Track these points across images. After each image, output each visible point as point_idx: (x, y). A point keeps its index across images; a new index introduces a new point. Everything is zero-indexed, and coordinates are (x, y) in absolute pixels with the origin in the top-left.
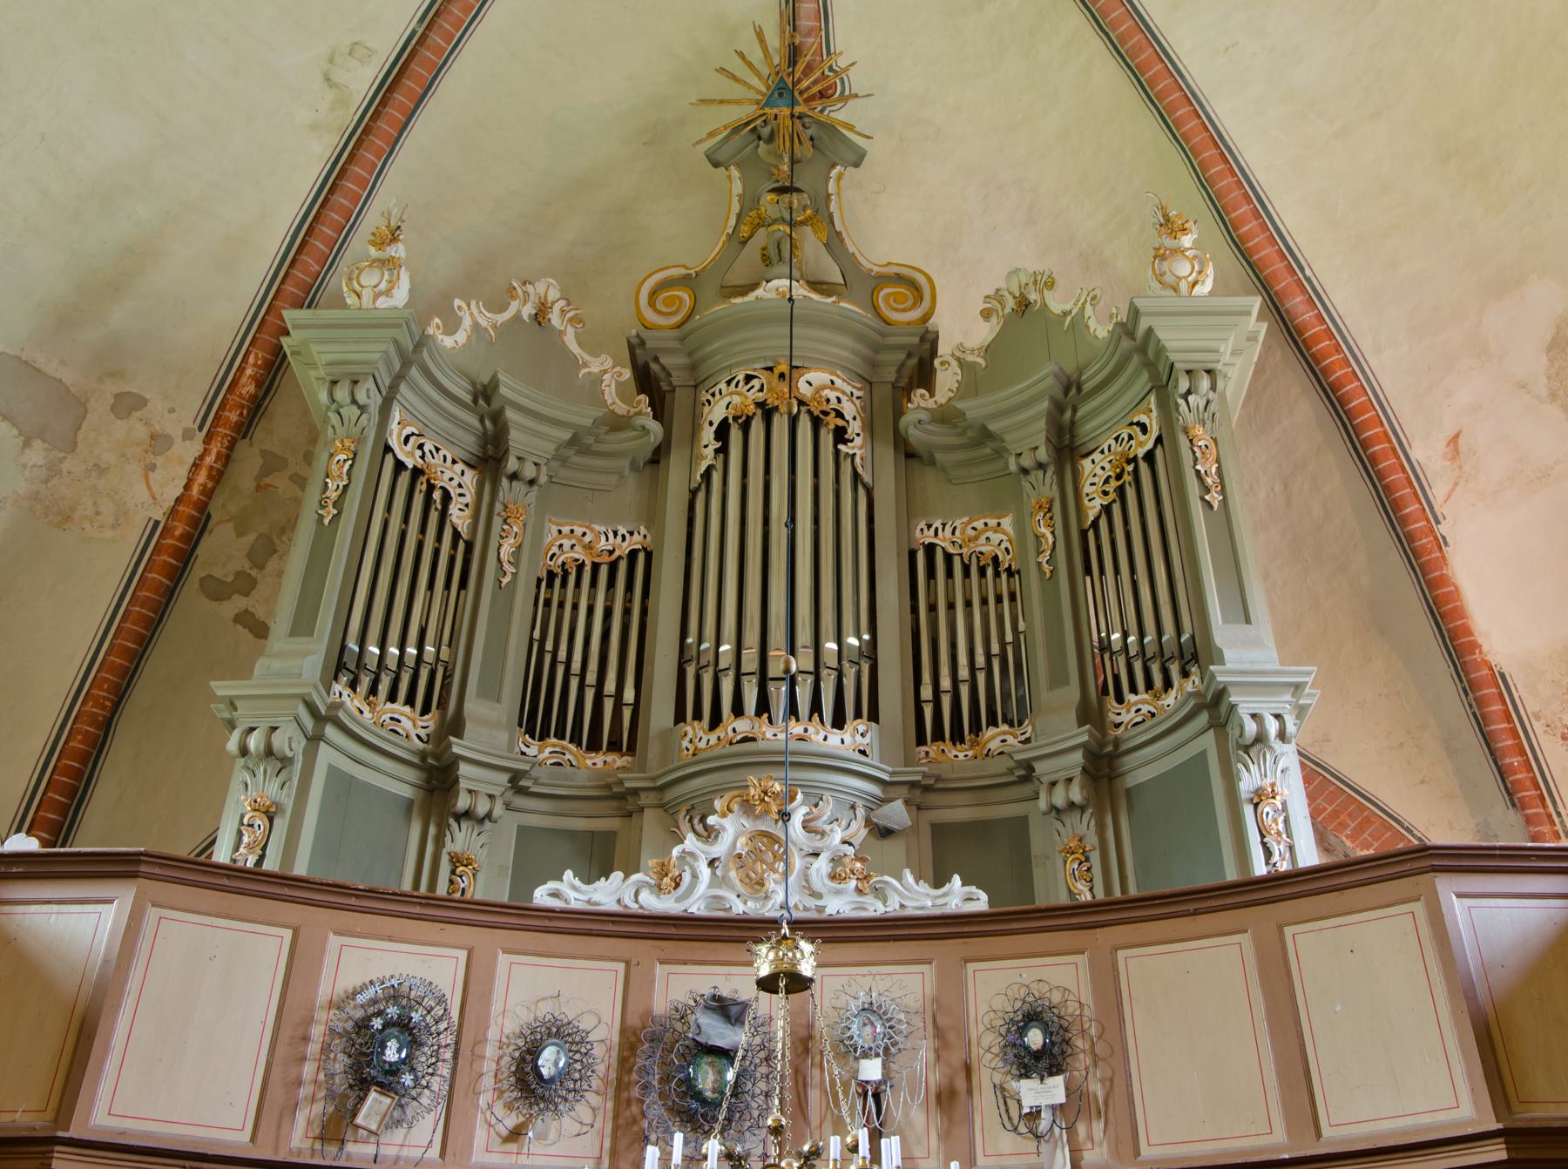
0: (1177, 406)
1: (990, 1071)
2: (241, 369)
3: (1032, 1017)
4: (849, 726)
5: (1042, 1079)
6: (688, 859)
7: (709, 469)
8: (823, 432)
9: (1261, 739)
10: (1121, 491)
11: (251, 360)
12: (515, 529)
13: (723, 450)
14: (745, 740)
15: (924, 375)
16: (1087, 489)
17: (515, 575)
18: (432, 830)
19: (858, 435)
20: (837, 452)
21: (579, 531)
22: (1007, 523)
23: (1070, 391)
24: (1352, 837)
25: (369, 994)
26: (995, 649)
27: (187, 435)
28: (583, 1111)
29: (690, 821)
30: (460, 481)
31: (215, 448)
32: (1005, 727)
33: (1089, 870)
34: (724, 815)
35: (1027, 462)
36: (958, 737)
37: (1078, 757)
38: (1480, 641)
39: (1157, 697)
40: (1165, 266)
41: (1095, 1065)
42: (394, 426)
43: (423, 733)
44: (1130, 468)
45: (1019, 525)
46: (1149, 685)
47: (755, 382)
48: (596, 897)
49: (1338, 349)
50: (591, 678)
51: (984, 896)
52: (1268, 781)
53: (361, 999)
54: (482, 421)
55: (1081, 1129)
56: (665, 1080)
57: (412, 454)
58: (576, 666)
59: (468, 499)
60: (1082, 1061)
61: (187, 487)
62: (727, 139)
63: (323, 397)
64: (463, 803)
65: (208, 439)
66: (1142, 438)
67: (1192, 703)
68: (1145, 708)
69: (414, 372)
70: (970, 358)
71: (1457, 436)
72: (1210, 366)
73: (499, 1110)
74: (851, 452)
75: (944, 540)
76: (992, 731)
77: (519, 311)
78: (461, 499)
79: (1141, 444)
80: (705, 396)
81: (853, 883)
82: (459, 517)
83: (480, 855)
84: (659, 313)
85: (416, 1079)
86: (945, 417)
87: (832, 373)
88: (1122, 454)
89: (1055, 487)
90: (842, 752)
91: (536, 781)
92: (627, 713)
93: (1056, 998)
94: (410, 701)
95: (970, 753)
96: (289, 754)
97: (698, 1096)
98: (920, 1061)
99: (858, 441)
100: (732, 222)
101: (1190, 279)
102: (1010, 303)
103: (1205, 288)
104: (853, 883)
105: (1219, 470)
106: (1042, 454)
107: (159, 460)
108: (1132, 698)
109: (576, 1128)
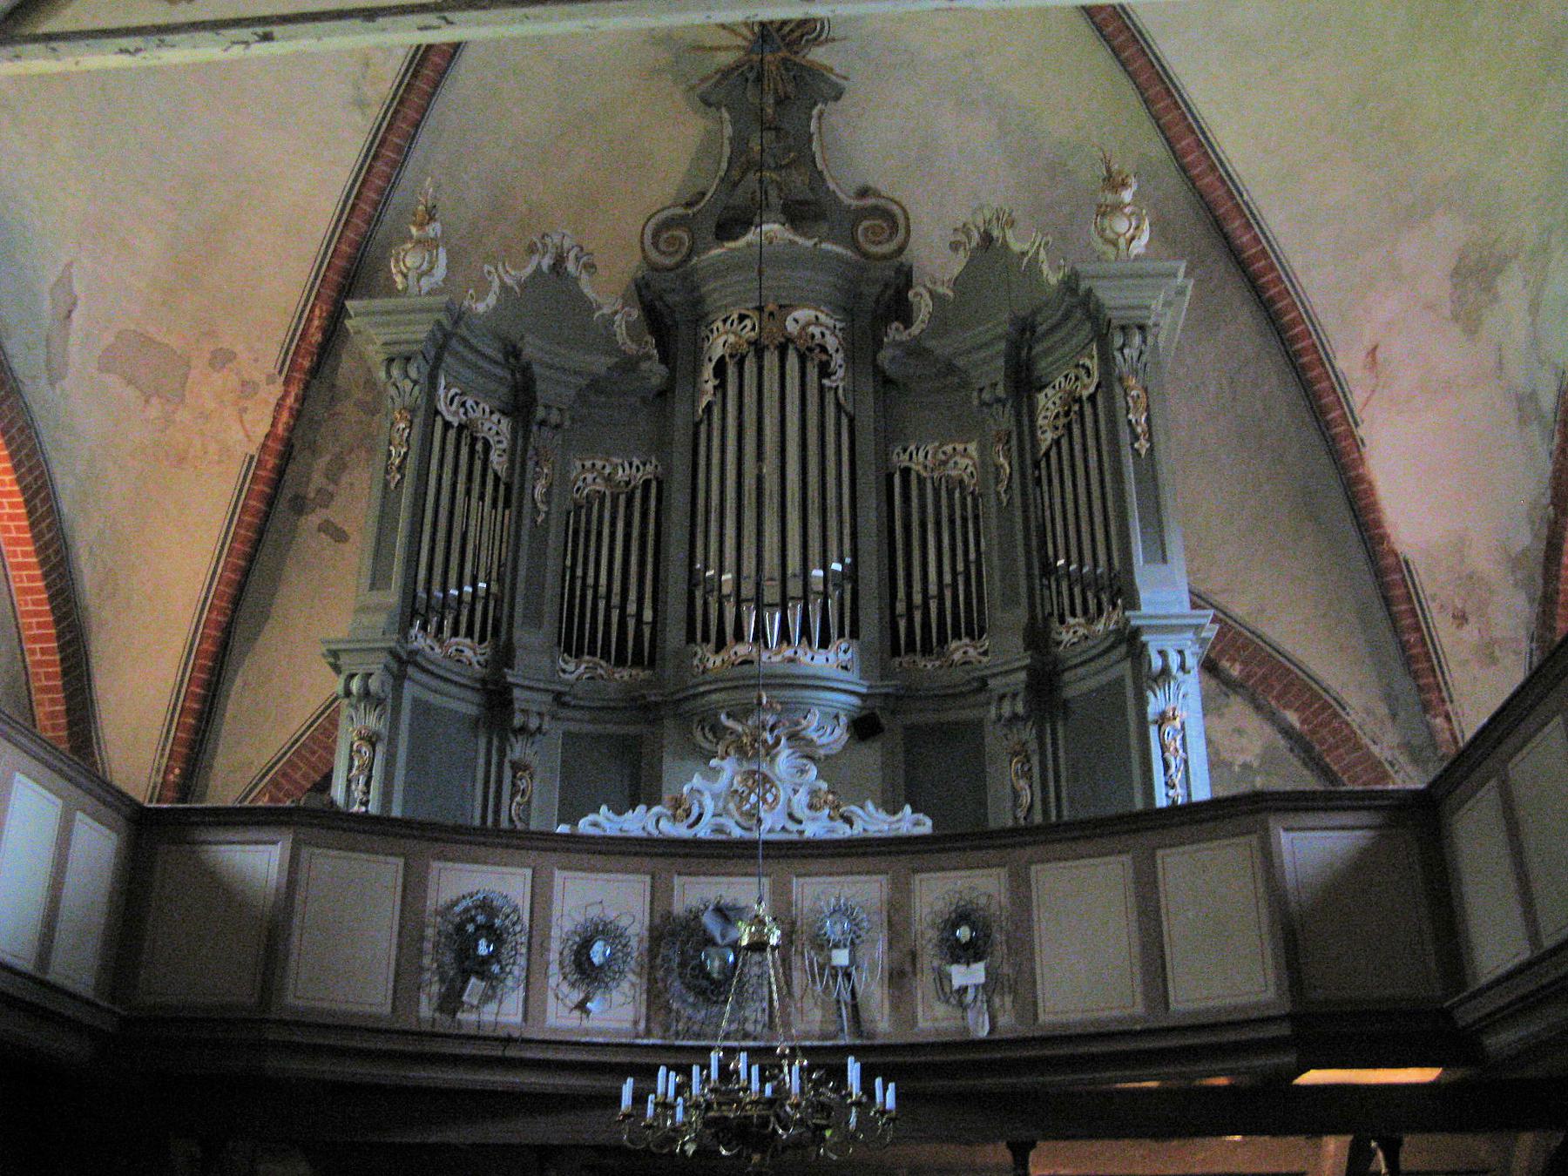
0: (1114, 358)
1: (929, 958)
2: (309, 320)
3: (963, 916)
4: (832, 647)
5: (968, 964)
6: (697, 794)
7: (709, 406)
8: (809, 365)
9: (1165, 671)
10: (1068, 427)
11: (317, 312)
12: (546, 471)
13: (721, 387)
14: (744, 663)
15: (901, 310)
16: (1040, 422)
17: (547, 513)
18: (495, 742)
19: (840, 366)
20: (822, 388)
21: (599, 464)
22: (972, 448)
23: (1025, 332)
24: (1277, 698)
25: (464, 904)
26: (960, 567)
27: (270, 380)
28: (625, 985)
29: (703, 729)
30: (497, 429)
31: (295, 391)
32: (966, 640)
33: (1030, 769)
34: (723, 758)
35: (986, 396)
36: (927, 650)
37: (1023, 676)
38: (1389, 531)
39: (1091, 621)
40: (1106, 222)
41: (1009, 954)
42: (441, 392)
43: (482, 659)
44: (1076, 408)
45: (982, 450)
46: (1085, 611)
47: (748, 322)
48: (626, 826)
49: (1272, 268)
50: (616, 600)
51: (929, 823)
52: (1171, 705)
53: (457, 909)
54: (513, 375)
55: (997, 1000)
56: (683, 965)
57: (456, 413)
58: (602, 590)
59: (505, 445)
60: (1000, 950)
61: (274, 425)
62: (718, 83)
63: (382, 375)
64: (518, 721)
65: (287, 382)
66: (1086, 380)
67: (1112, 639)
68: (1081, 631)
69: (454, 342)
70: (941, 290)
71: (1375, 349)
72: (1142, 322)
73: (565, 988)
74: (834, 385)
75: (918, 464)
76: (954, 645)
77: (539, 263)
78: (500, 446)
79: (1085, 387)
80: (704, 332)
81: (826, 811)
82: (498, 462)
83: (535, 762)
84: (663, 253)
85: (501, 968)
86: (915, 351)
87: (817, 309)
88: (1070, 393)
89: (1013, 419)
90: (825, 673)
91: (575, 697)
92: (647, 631)
93: (983, 901)
94: (470, 633)
95: (937, 663)
96: (382, 695)
97: (707, 976)
98: (877, 951)
99: (841, 373)
100: (724, 165)
101: (1128, 235)
102: (976, 237)
103: (1139, 247)
104: (826, 811)
105: (1148, 419)
106: (1001, 391)
107: (249, 404)
108: (1071, 621)
109: (622, 999)
